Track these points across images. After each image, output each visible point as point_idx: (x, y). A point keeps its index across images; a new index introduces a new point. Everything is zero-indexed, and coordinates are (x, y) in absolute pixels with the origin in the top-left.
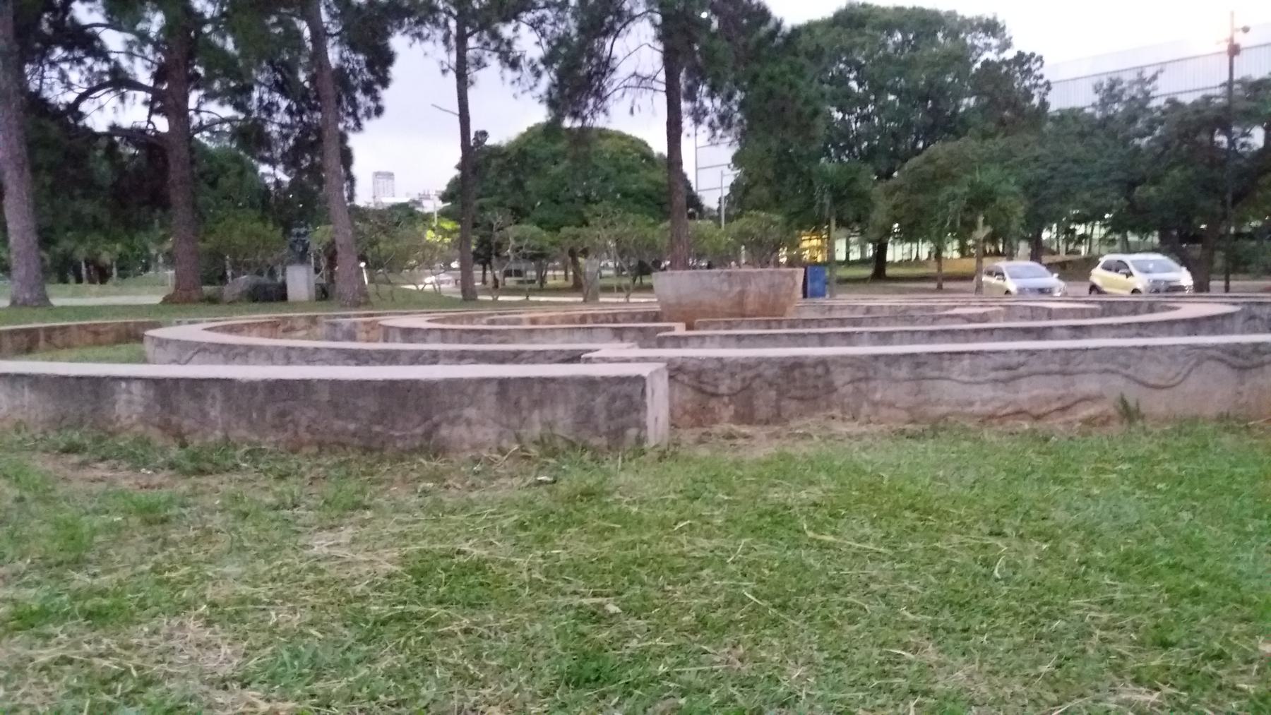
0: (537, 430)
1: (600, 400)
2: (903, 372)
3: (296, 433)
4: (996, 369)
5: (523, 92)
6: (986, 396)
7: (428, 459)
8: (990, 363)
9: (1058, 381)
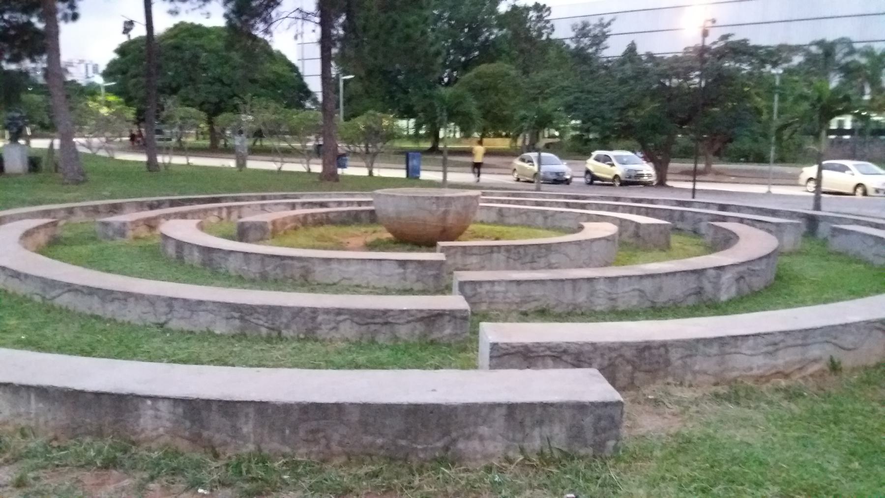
0: (537, 444)
1: (588, 421)
2: (714, 350)
3: (328, 446)
4: (767, 345)
5: (193, 9)
6: (759, 363)
7: (447, 467)
8: (764, 341)
9: (799, 349)
